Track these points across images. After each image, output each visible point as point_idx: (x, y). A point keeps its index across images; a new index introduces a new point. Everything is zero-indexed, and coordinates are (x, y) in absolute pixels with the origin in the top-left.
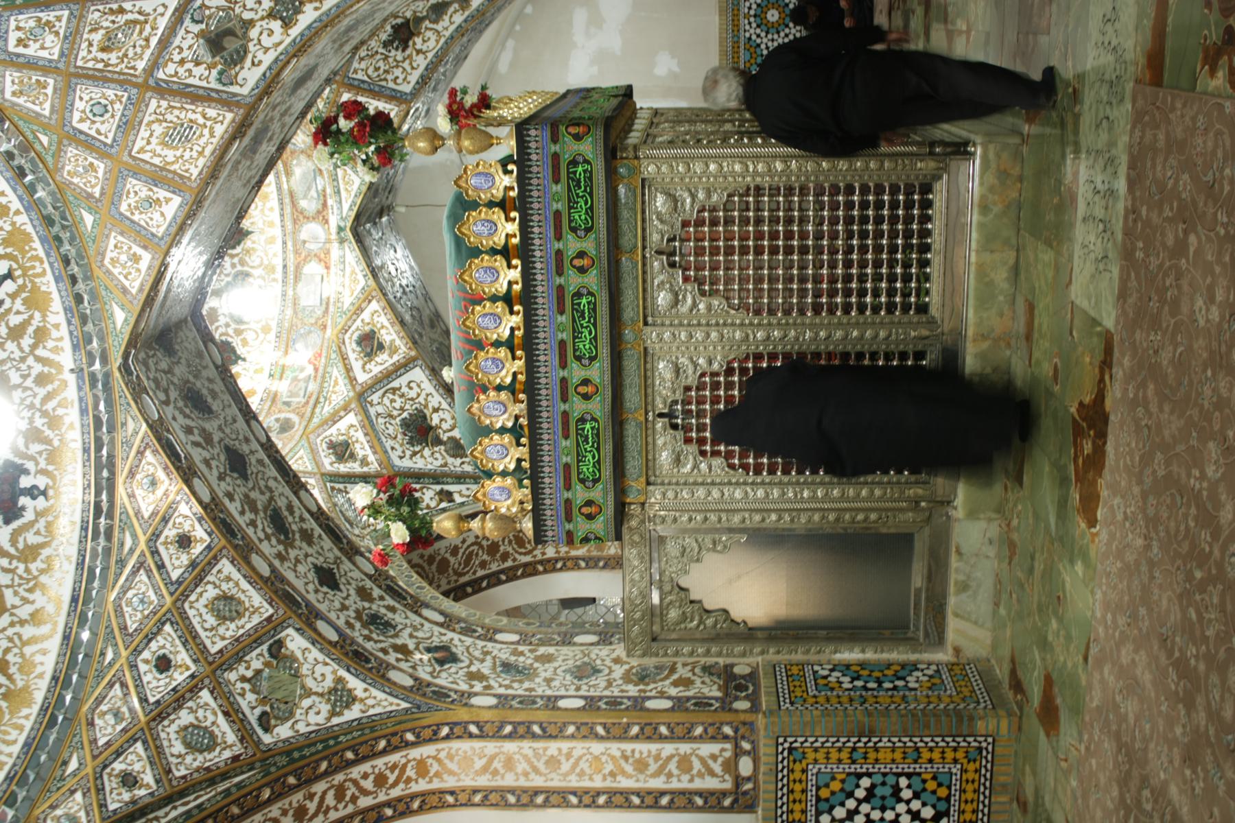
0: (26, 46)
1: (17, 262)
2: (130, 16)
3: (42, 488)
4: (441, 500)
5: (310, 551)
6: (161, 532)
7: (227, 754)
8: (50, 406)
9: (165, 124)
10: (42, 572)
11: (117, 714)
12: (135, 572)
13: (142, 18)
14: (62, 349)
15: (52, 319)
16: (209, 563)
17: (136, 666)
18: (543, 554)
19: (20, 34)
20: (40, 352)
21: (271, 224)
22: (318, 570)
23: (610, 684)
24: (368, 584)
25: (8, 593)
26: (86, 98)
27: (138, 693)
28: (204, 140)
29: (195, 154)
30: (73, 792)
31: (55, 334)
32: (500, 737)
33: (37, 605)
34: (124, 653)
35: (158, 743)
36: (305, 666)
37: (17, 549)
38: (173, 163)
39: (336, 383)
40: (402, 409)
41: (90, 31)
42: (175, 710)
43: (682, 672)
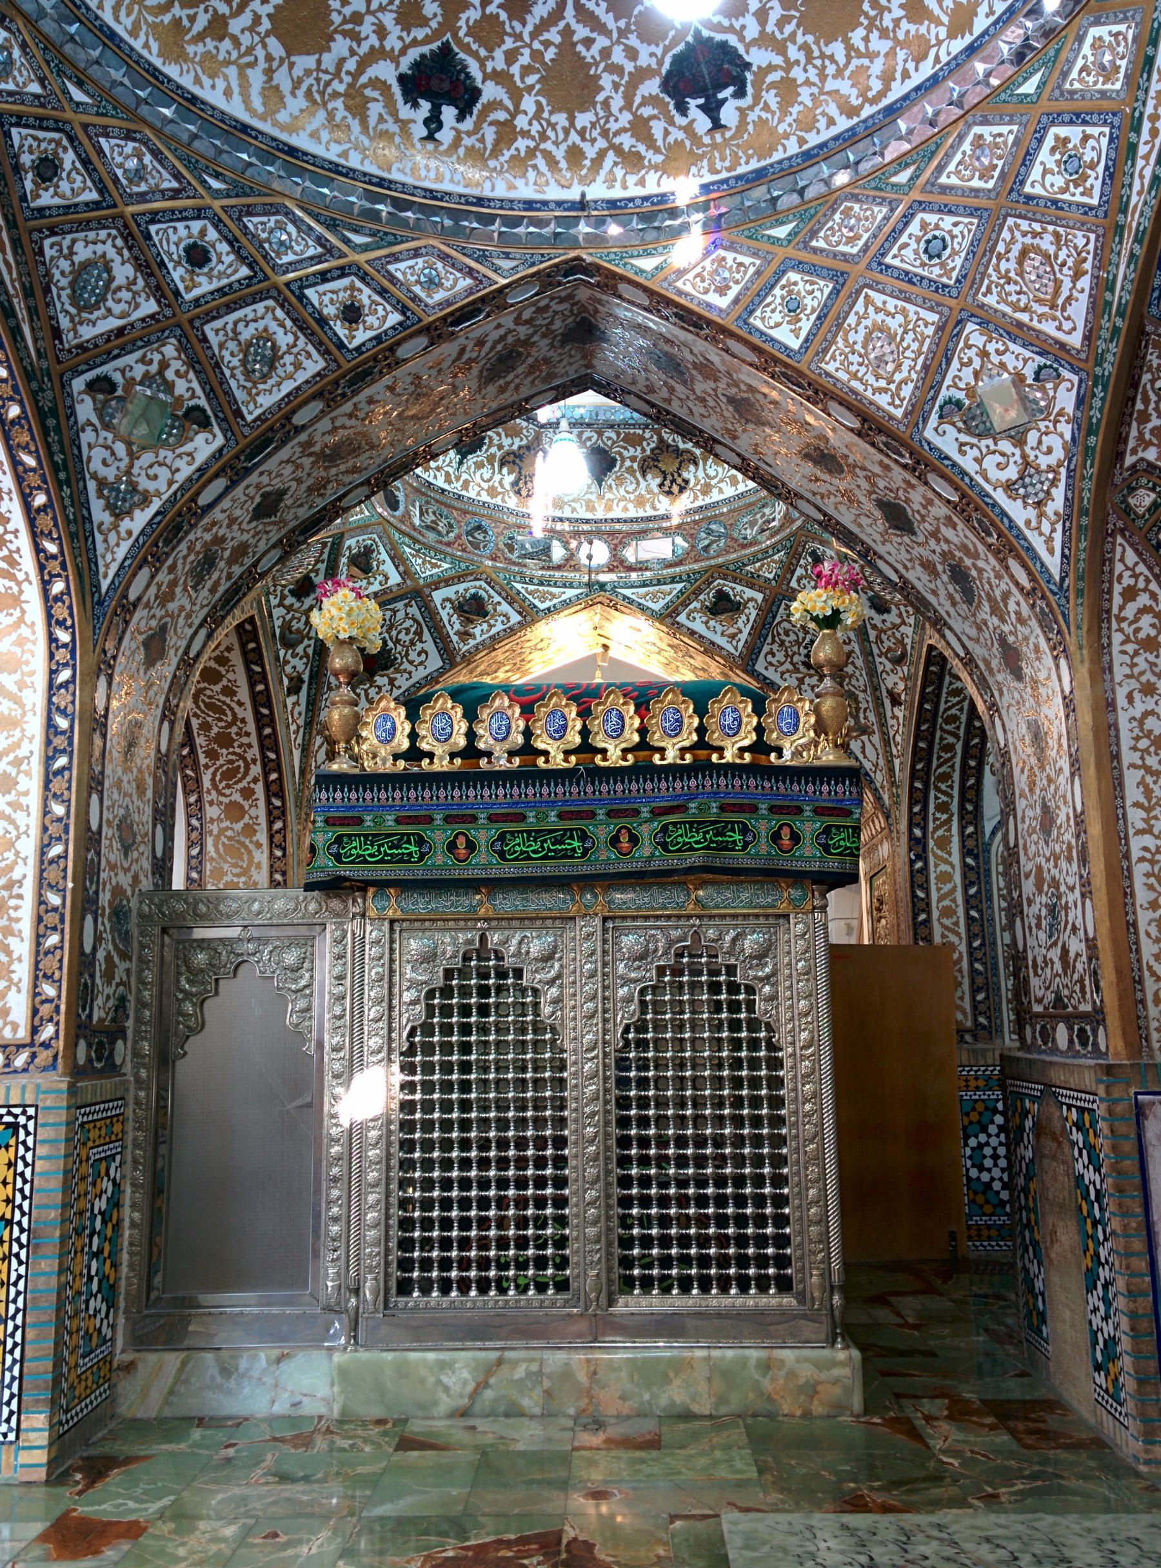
0: (1053, 150)
1: (732, 138)
2: (1067, 284)
3: (437, 136)
4: (291, 679)
5: (304, 487)
6: (368, 284)
7: (65, 323)
8: (540, 162)
9: (900, 331)
10: (331, 116)
11: (139, 175)
12: (320, 241)
13: (1060, 302)
14: (611, 187)
15: (652, 177)
16: (321, 343)
17: (198, 218)
18: (211, 803)
19: (1075, 140)
20: (611, 157)
21: (609, 508)
22: (281, 494)
23: (113, 867)
24: (248, 561)
25: (309, 61)
26: (956, 231)
27: (164, 211)
28: (871, 379)
29: (853, 368)
30: (42, 81)
31: (632, 179)
32: (49, 712)
33: (289, 99)
34: (217, 204)
35: (93, 225)
36: (169, 454)
37: (365, 86)
38: (846, 340)
39: (434, 566)
40: (397, 641)
41: (1057, 235)
42: (136, 259)
43: (122, 966)
